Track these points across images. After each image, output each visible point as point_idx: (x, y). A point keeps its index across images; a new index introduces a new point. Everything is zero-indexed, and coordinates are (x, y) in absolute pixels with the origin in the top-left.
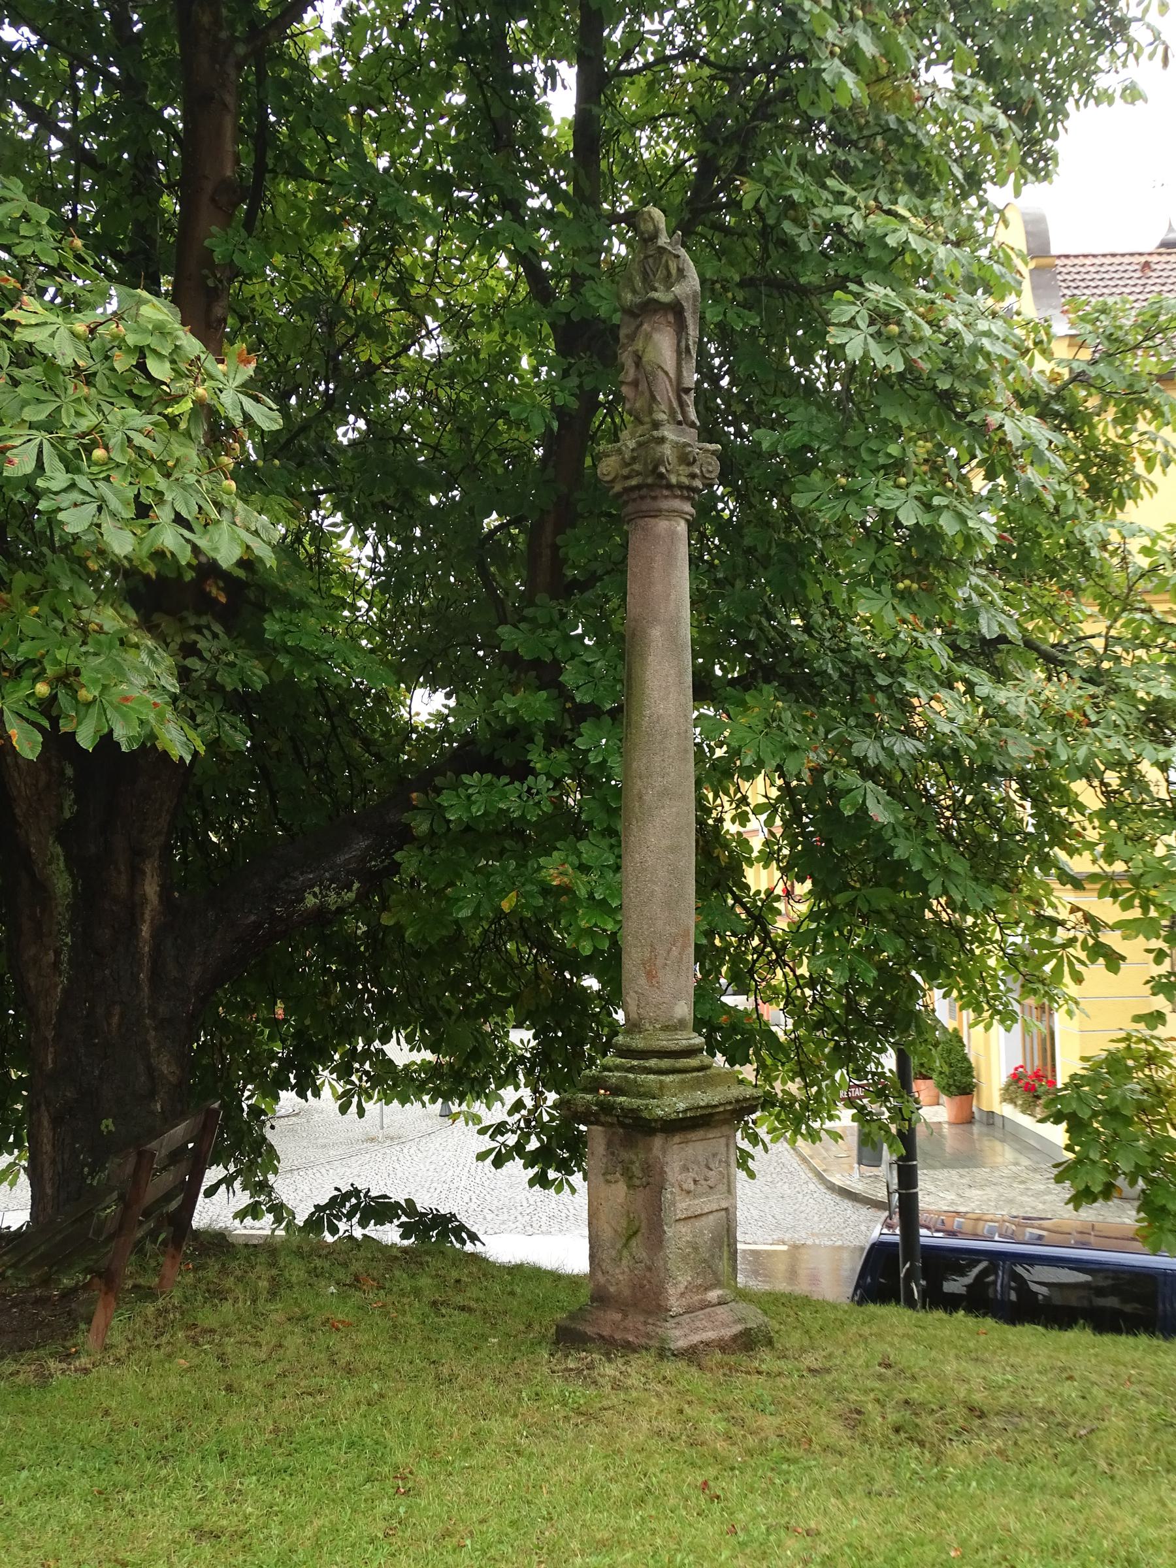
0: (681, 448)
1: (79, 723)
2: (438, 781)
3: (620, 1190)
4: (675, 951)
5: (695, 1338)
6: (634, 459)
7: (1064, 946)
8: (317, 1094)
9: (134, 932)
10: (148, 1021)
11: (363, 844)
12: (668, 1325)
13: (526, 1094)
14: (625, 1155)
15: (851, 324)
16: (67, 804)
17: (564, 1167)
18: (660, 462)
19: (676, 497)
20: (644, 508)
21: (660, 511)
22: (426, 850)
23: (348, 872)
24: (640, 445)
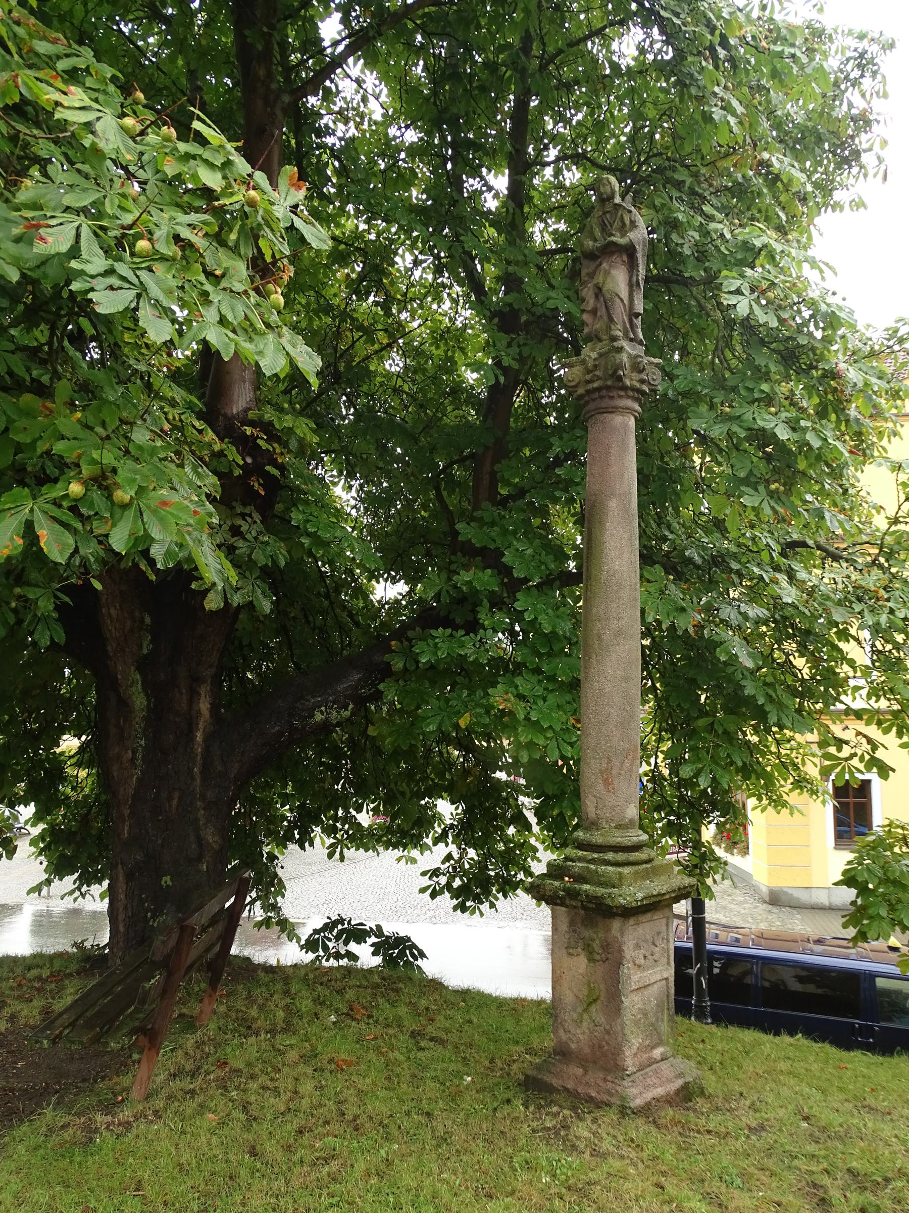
0: (634, 359)
1: (114, 525)
2: (410, 634)
3: (580, 963)
4: (627, 763)
5: (649, 1096)
6: (595, 366)
7: (847, 759)
8: (312, 844)
9: (191, 738)
10: (199, 803)
11: (356, 677)
12: (625, 1083)
13: (453, 848)
14: (587, 933)
15: (738, 292)
16: (145, 644)
17: (478, 899)
18: (620, 366)
19: (629, 397)
20: (603, 405)
21: (617, 408)
22: (401, 683)
23: (346, 697)
24: (601, 355)
